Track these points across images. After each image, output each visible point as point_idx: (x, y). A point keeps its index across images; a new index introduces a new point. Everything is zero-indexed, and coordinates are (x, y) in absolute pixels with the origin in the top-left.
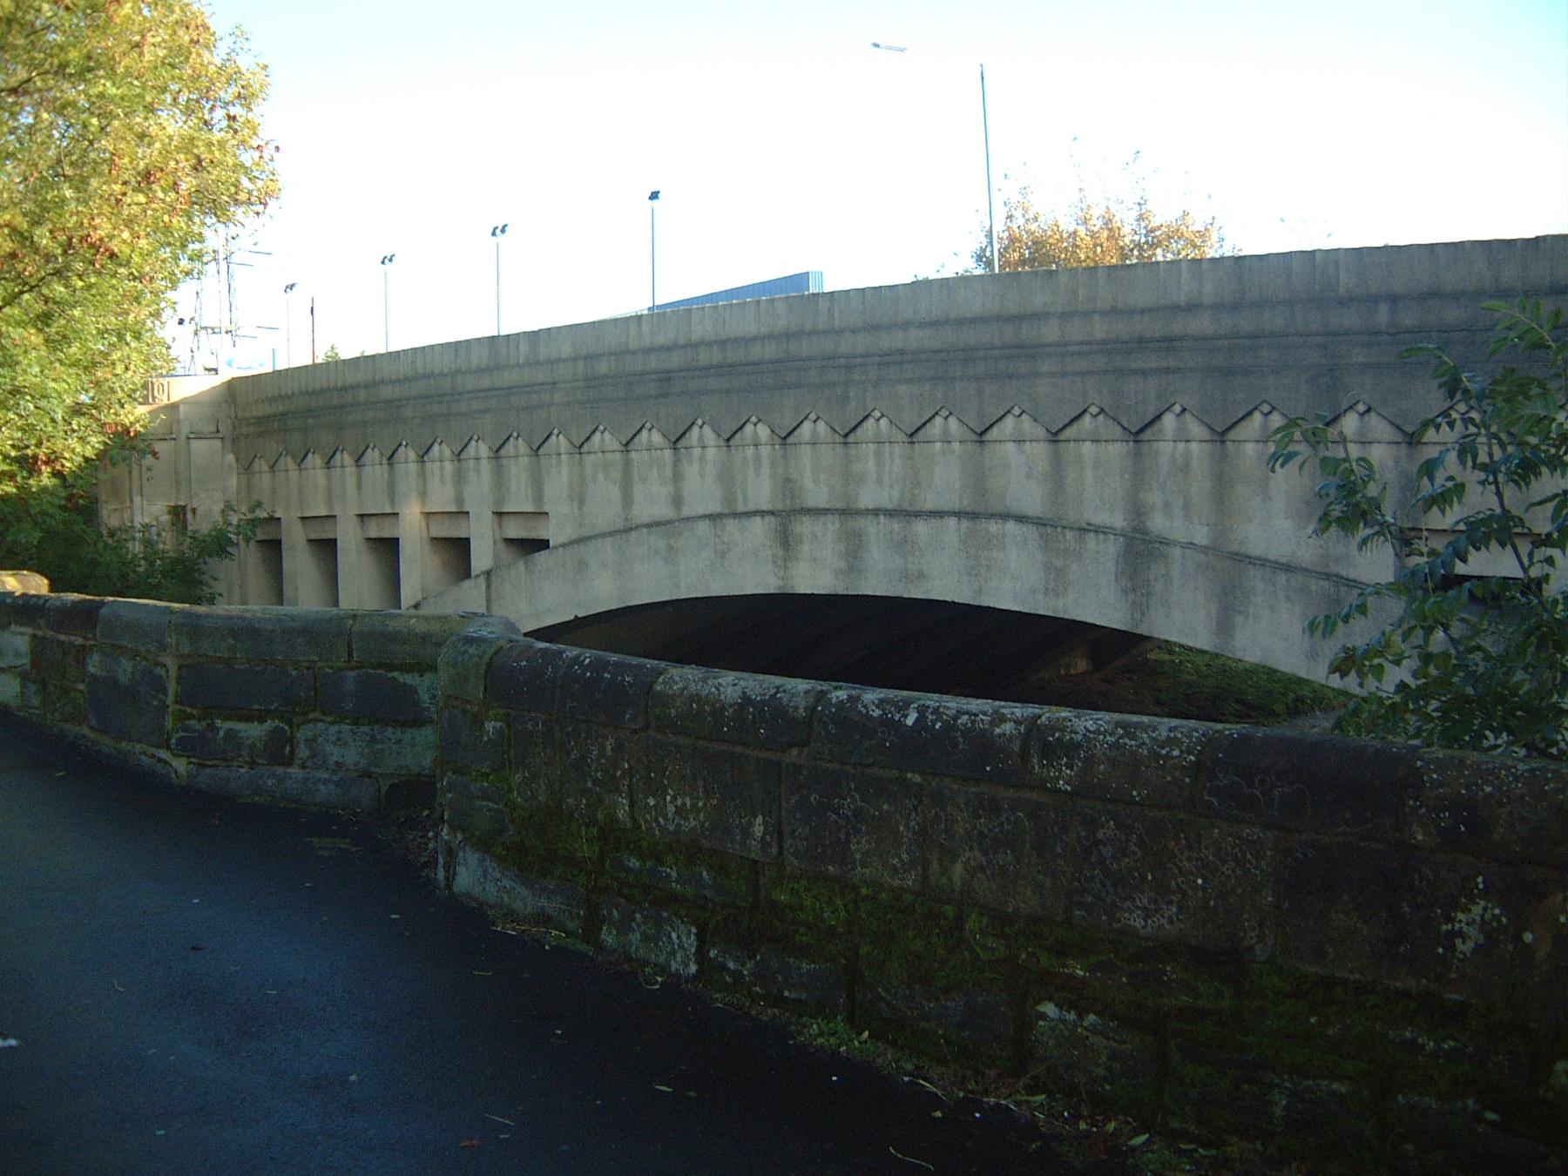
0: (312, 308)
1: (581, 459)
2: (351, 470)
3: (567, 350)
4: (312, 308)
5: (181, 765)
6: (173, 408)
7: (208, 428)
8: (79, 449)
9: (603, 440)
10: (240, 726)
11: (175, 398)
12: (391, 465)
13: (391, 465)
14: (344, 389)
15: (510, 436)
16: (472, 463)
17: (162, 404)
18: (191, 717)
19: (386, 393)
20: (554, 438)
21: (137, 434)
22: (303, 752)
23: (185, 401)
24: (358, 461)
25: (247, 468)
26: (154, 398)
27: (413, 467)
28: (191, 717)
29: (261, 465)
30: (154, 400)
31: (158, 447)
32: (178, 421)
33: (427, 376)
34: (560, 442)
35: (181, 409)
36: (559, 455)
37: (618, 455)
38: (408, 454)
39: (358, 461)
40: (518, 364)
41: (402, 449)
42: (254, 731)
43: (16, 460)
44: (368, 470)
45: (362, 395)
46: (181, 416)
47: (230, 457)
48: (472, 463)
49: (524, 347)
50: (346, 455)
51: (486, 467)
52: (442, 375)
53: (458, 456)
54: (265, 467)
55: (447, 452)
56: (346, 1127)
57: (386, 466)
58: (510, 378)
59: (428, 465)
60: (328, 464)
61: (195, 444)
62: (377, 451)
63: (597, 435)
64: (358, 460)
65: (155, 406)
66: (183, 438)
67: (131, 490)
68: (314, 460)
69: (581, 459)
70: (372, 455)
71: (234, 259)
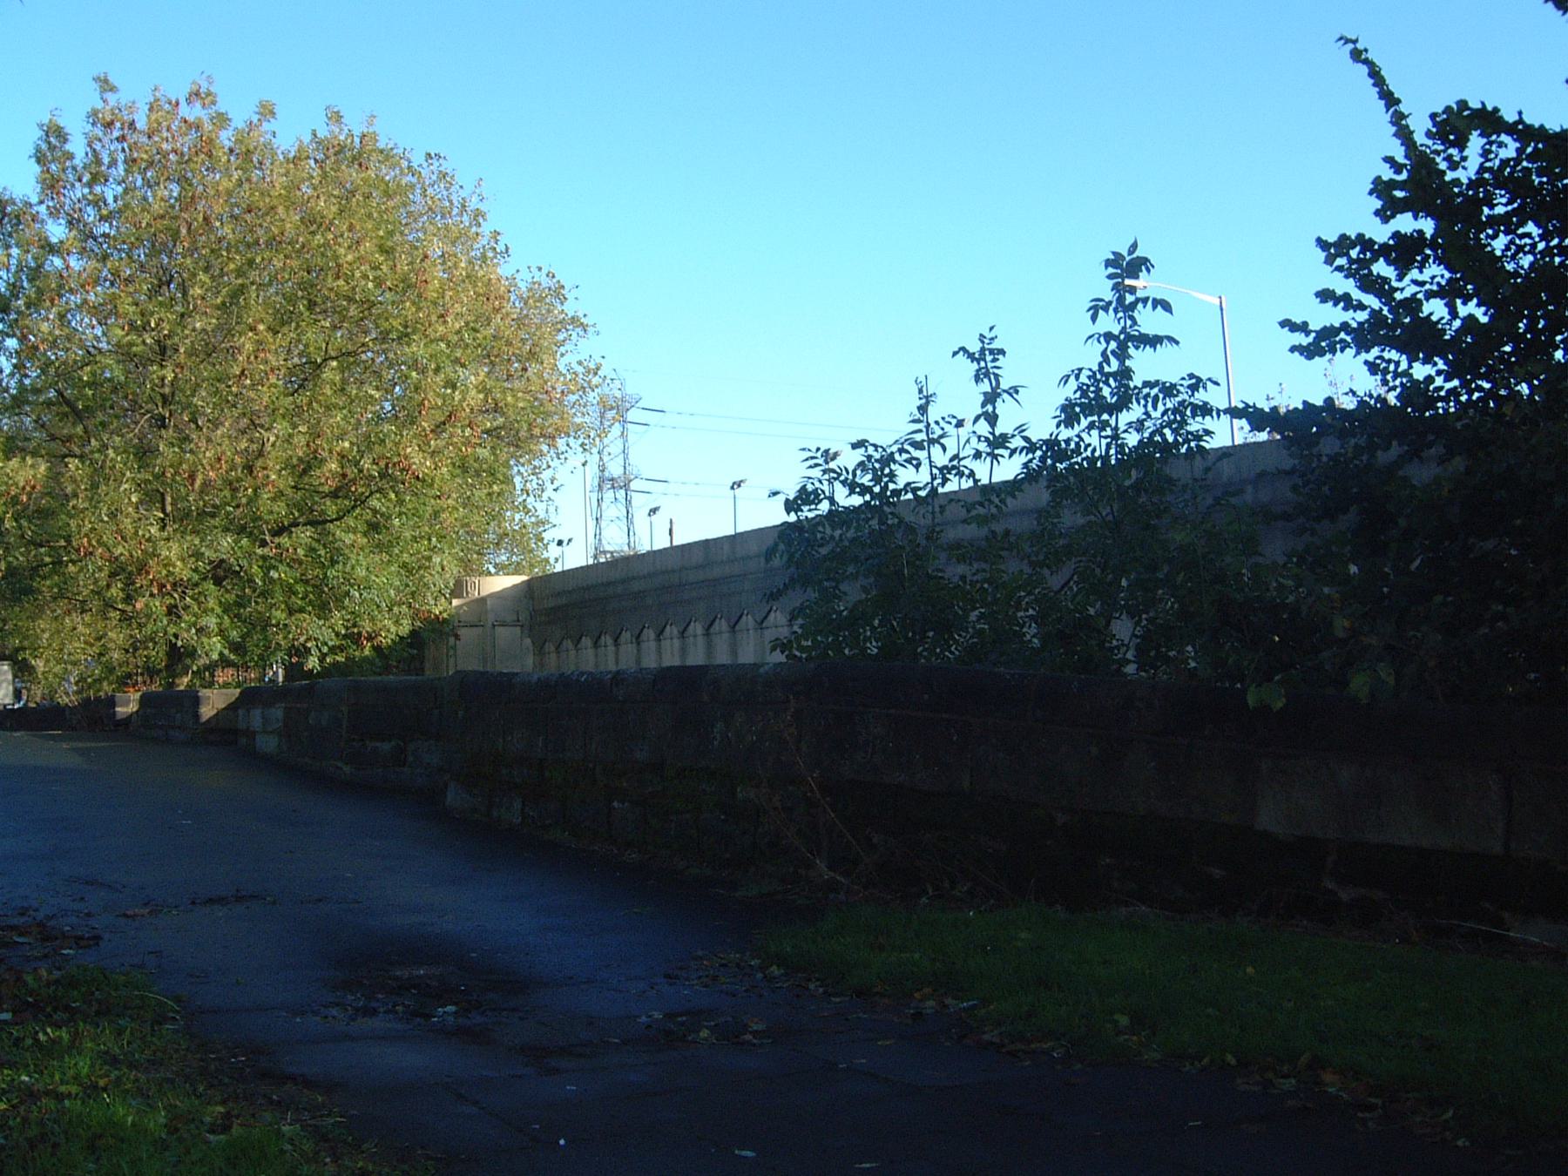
0: (671, 531)
1: (762, 633)
2: (611, 648)
3: (754, 548)
4: (671, 531)
5: (347, 769)
6: (483, 600)
7: (510, 618)
8: (393, 629)
9: (776, 618)
10: (378, 744)
11: (483, 594)
12: (638, 644)
13: (638, 644)
14: (609, 584)
15: (716, 617)
16: (691, 638)
17: (473, 598)
18: (354, 739)
19: (636, 586)
20: (744, 617)
21: (444, 619)
22: (411, 759)
23: (492, 595)
24: (616, 640)
25: (540, 650)
26: (467, 593)
27: (653, 644)
28: (354, 739)
29: (549, 647)
30: (467, 593)
31: (462, 632)
32: (486, 612)
33: (663, 573)
34: (748, 621)
35: (488, 602)
36: (748, 630)
37: (786, 628)
38: (650, 634)
39: (616, 640)
40: (722, 562)
41: (645, 630)
42: (386, 747)
43: (345, 637)
44: (622, 648)
45: (620, 589)
46: (489, 607)
47: (528, 641)
48: (691, 638)
49: (726, 547)
50: (608, 637)
51: (701, 641)
52: (673, 571)
53: (682, 634)
54: (553, 649)
55: (675, 632)
56: (155, 620)
57: (634, 645)
58: (717, 572)
59: (663, 642)
60: (596, 645)
61: (499, 630)
62: (628, 633)
63: (772, 615)
64: (616, 641)
65: (467, 600)
66: (490, 625)
67: (447, 666)
68: (586, 642)
69: (762, 633)
70: (626, 636)
71: (633, 485)
